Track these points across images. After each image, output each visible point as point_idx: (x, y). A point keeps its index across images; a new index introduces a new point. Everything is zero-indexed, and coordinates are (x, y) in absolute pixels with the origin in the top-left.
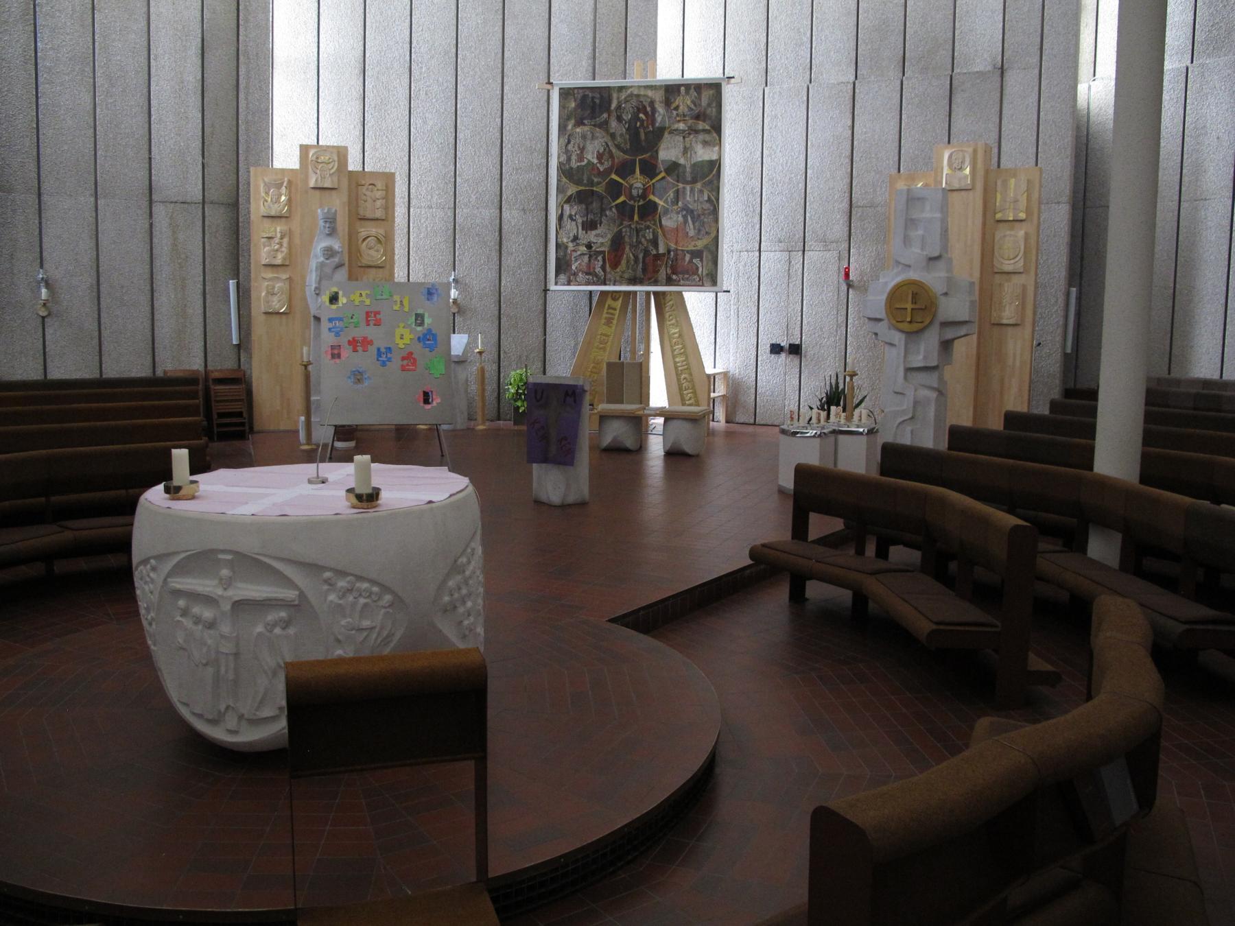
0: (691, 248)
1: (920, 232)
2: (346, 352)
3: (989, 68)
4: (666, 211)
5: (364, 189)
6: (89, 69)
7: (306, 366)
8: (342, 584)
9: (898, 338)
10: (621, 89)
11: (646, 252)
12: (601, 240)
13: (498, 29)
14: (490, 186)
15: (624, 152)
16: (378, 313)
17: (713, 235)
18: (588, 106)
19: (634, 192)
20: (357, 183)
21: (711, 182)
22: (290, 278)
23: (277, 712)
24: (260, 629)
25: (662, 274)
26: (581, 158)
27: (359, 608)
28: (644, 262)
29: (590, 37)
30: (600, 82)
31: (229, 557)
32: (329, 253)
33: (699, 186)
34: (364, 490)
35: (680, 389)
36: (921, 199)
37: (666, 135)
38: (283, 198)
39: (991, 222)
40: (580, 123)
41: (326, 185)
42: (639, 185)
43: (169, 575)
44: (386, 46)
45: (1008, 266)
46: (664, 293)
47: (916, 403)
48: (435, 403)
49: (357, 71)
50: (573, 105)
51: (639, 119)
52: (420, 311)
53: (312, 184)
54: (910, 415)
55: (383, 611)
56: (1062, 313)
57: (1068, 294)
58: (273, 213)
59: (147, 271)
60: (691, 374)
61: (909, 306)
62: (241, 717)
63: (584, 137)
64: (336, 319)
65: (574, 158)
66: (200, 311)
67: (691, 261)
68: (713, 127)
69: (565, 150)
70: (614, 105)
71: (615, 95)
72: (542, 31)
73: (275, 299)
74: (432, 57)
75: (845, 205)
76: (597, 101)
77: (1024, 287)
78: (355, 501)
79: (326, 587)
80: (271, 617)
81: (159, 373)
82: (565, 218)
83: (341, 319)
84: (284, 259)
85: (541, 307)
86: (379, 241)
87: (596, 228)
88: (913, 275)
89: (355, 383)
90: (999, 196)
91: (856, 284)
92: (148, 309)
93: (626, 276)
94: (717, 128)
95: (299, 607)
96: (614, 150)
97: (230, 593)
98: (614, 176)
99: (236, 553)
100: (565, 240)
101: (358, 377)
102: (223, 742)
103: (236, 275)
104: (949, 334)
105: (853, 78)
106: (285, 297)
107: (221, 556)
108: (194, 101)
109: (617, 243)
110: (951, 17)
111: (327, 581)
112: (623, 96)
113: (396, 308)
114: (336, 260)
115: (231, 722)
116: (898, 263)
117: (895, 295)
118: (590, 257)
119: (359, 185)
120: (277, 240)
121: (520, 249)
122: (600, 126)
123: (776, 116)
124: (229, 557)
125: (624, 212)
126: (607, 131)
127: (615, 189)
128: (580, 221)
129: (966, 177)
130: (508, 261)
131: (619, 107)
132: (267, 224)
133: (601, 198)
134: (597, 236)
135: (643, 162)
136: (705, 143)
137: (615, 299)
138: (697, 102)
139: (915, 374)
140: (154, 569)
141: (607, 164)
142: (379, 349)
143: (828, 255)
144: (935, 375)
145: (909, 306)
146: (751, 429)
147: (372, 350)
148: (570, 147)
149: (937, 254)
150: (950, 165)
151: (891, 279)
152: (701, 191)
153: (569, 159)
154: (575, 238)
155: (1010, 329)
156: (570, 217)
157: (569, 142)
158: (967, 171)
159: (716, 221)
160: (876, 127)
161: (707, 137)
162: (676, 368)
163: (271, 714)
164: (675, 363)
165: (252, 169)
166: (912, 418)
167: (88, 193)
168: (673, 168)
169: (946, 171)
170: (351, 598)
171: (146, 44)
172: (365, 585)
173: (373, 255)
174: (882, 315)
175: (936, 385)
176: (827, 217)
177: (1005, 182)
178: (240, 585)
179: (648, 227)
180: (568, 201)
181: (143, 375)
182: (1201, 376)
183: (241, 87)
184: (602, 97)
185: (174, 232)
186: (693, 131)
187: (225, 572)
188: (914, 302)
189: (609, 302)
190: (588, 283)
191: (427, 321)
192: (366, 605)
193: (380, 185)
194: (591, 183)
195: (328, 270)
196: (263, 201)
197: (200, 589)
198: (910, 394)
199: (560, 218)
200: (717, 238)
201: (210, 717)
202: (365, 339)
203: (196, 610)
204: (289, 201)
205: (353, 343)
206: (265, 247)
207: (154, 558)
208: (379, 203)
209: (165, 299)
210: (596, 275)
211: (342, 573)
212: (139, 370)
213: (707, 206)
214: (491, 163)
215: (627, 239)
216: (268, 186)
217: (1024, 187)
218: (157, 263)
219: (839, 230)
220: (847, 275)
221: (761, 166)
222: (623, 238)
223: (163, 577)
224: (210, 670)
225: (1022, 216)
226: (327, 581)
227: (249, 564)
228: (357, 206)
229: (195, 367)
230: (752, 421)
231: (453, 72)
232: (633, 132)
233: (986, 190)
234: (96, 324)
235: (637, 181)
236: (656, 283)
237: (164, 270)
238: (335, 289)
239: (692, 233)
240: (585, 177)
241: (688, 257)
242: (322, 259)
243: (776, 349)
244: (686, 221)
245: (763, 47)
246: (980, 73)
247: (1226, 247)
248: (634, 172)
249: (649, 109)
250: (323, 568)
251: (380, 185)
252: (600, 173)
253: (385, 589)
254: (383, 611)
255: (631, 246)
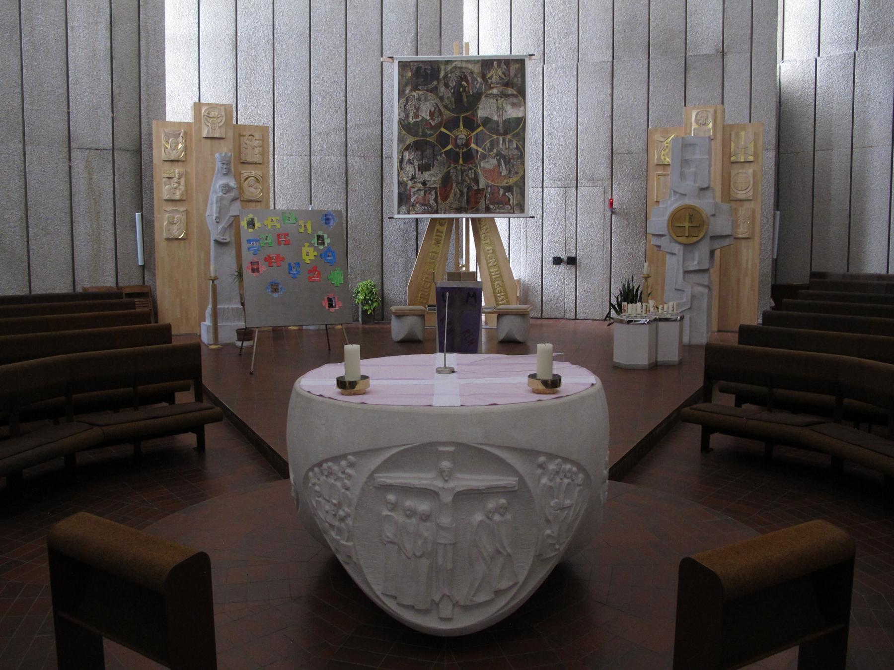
0: (504, 184)
1: (693, 170)
2: (263, 268)
3: (713, 52)
4: (484, 157)
5: (245, 139)
6: (16, 36)
7: (213, 281)
8: (552, 467)
9: (677, 249)
10: (447, 62)
11: (469, 188)
12: (433, 179)
13: (342, 16)
14: (339, 138)
15: (449, 110)
16: (286, 235)
17: (520, 175)
18: (420, 76)
19: (459, 142)
20: (240, 133)
21: (518, 134)
22: (187, 212)
23: (493, 596)
24: (479, 517)
25: (482, 205)
26: (416, 115)
27: (564, 487)
28: (467, 195)
29: (413, 24)
30: (422, 57)
31: (452, 449)
32: (227, 189)
33: (509, 137)
34: (549, 377)
35: (495, 293)
36: (693, 145)
37: (483, 98)
38: (180, 146)
39: (729, 163)
40: (415, 88)
41: (215, 136)
42: (463, 136)
43: (378, 470)
44: (254, 25)
45: (741, 195)
46: (480, 219)
47: (693, 297)
48: (337, 308)
49: (231, 47)
50: (410, 74)
51: (462, 86)
52: (320, 233)
53: (205, 134)
54: (688, 307)
55: (578, 489)
56: (771, 229)
57: (774, 217)
58: (172, 158)
59: (68, 205)
60: (503, 281)
61: (687, 225)
62: (456, 605)
63: (419, 99)
64: (253, 240)
65: (411, 115)
66: (112, 238)
67: (504, 195)
68: (519, 93)
69: (404, 109)
70: (442, 75)
71: (443, 67)
72: (376, 19)
73: (175, 227)
74: (291, 37)
75: (608, 153)
76: (429, 72)
77: (754, 212)
78: (541, 387)
79: (539, 471)
80: (491, 505)
81: (79, 289)
82: (405, 162)
83: (258, 241)
84: (182, 195)
85: (378, 232)
86: (257, 180)
87: (429, 169)
88: (688, 201)
89: (272, 292)
90: (733, 145)
91: (617, 210)
92: (69, 237)
93: (454, 206)
94: (522, 92)
95: (516, 494)
96: (443, 110)
97: (451, 484)
98: (443, 130)
99: (458, 444)
100: (405, 179)
101: (275, 288)
102: (439, 630)
103: (141, 209)
104: (717, 244)
105: (611, 59)
106: (183, 226)
107: (441, 449)
108: (105, 66)
109: (446, 180)
110: (684, 15)
111: (542, 466)
112: (449, 68)
113: (302, 230)
114: (233, 194)
115: (446, 610)
116: (675, 192)
117: (675, 218)
118: (425, 192)
119: (241, 136)
120: (175, 180)
121: (362, 187)
122: (431, 91)
123: (553, 86)
124: (452, 449)
125: (453, 157)
126: (437, 94)
127: (443, 140)
128: (417, 164)
129: (709, 130)
130: (352, 197)
131: (446, 76)
132: (167, 166)
133: (433, 146)
134: (430, 175)
135: (465, 118)
136: (514, 105)
137: (442, 225)
138: (507, 73)
139: (692, 276)
140: (351, 465)
141: (437, 120)
142: (289, 265)
143: (595, 190)
144: (706, 276)
145: (687, 225)
146: (539, 322)
147: (285, 265)
148: (408, 107)
149: (705, 186)
150: (697, 121)
151: (671, 205)
152: (510, 141)
153: (407, 116)
154: (413, 178)
155: (743, 241)
156: (409, 161)
157: (407, 103)
158: (711, 125)
159: (523, 163)
160: (630, 94)
161: (515, 100)
162: (491, 276)
163: (487, 598)
164: (490, 273)
165: (154, 123)
166: (690, 308)
167: (17, 140)
168: (487, 121)
169: (694, 126)
170: (558, 480)
171: (64, 18)
172: (568, 466)
173: (253, 191)
174: (664, 231)
175: (706, 283)
176: (594, 161)
177: (737, 134)
178: (459, 476)
179: (471, 169)
180: (407, 149)
181: (65, 291)
182: (872, 272)
183: (142, 56)
184: (432, 69)
185: (89, 173)
186: (504, 95)
187: (446, 464)
188: (691, 221)
189: (438, 227)
190: (424, 213)
191: (327, 241)
192: (569, 484)
193: (257, 135)
194: (424, 135)
195: (226, 203)
196: (164, 148)
197: (416, 482)
198: (689, 291)
199: (401, 162)
200: (523, 177)
201: (423, 607)
202: (278, 256)
203: (409, 503)
204: (186, 148)
205: (268, 259)
206: (165, 187)
207: (353, 454)
208: (257, 150)
209: (82, 229)
210: (431, 206)
211: (552, 456)
212: (60, 286)
213: (516, 152)
214: (337, 121)
215: (454, 178)
216: (168, 136)
217: (751, 137)
218: (75, 199)
219: (603, 170)
220: (611, 204)
221: (555, 119)
222: (451, 177)
223: (367, 473)
224: (425, 562)
225: (751, 158)
226: (542, 466)
227: (470, 454)
228: (240, 153)
229: (108, 285)
230: (539, 316)
231: (308, 48)
232: (458, 95)
233: (723, 140)
234: (25, 250)
235: (462, 133)
236: (477, 211)
237: (81, 207)
238: (251, 216)
239: (504, 173)
240: (420, 130)
241: (501, 191)
242: (220, 194)
243: (557, 261)
244: (499, 164)
245: (541, 34)
246: (707, 56)
247: (888, 180)
248: (459, 127)
249: (469, 78)
250: (539, 453)
251: (257, 135)
252: (432, 127)
253: (581, 468)
254: (578, 489)
255: (458, 183)
